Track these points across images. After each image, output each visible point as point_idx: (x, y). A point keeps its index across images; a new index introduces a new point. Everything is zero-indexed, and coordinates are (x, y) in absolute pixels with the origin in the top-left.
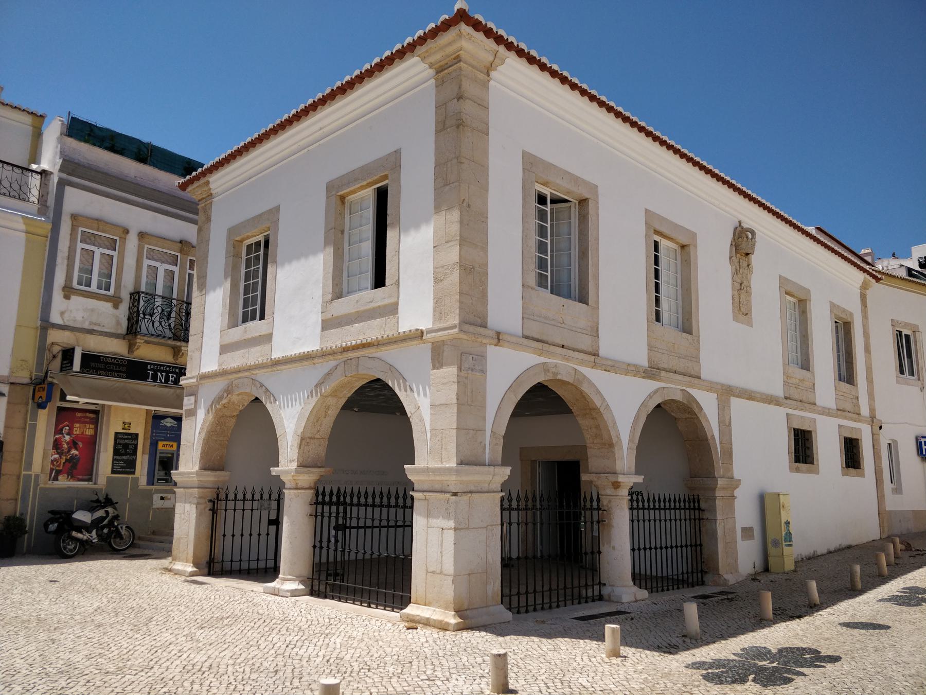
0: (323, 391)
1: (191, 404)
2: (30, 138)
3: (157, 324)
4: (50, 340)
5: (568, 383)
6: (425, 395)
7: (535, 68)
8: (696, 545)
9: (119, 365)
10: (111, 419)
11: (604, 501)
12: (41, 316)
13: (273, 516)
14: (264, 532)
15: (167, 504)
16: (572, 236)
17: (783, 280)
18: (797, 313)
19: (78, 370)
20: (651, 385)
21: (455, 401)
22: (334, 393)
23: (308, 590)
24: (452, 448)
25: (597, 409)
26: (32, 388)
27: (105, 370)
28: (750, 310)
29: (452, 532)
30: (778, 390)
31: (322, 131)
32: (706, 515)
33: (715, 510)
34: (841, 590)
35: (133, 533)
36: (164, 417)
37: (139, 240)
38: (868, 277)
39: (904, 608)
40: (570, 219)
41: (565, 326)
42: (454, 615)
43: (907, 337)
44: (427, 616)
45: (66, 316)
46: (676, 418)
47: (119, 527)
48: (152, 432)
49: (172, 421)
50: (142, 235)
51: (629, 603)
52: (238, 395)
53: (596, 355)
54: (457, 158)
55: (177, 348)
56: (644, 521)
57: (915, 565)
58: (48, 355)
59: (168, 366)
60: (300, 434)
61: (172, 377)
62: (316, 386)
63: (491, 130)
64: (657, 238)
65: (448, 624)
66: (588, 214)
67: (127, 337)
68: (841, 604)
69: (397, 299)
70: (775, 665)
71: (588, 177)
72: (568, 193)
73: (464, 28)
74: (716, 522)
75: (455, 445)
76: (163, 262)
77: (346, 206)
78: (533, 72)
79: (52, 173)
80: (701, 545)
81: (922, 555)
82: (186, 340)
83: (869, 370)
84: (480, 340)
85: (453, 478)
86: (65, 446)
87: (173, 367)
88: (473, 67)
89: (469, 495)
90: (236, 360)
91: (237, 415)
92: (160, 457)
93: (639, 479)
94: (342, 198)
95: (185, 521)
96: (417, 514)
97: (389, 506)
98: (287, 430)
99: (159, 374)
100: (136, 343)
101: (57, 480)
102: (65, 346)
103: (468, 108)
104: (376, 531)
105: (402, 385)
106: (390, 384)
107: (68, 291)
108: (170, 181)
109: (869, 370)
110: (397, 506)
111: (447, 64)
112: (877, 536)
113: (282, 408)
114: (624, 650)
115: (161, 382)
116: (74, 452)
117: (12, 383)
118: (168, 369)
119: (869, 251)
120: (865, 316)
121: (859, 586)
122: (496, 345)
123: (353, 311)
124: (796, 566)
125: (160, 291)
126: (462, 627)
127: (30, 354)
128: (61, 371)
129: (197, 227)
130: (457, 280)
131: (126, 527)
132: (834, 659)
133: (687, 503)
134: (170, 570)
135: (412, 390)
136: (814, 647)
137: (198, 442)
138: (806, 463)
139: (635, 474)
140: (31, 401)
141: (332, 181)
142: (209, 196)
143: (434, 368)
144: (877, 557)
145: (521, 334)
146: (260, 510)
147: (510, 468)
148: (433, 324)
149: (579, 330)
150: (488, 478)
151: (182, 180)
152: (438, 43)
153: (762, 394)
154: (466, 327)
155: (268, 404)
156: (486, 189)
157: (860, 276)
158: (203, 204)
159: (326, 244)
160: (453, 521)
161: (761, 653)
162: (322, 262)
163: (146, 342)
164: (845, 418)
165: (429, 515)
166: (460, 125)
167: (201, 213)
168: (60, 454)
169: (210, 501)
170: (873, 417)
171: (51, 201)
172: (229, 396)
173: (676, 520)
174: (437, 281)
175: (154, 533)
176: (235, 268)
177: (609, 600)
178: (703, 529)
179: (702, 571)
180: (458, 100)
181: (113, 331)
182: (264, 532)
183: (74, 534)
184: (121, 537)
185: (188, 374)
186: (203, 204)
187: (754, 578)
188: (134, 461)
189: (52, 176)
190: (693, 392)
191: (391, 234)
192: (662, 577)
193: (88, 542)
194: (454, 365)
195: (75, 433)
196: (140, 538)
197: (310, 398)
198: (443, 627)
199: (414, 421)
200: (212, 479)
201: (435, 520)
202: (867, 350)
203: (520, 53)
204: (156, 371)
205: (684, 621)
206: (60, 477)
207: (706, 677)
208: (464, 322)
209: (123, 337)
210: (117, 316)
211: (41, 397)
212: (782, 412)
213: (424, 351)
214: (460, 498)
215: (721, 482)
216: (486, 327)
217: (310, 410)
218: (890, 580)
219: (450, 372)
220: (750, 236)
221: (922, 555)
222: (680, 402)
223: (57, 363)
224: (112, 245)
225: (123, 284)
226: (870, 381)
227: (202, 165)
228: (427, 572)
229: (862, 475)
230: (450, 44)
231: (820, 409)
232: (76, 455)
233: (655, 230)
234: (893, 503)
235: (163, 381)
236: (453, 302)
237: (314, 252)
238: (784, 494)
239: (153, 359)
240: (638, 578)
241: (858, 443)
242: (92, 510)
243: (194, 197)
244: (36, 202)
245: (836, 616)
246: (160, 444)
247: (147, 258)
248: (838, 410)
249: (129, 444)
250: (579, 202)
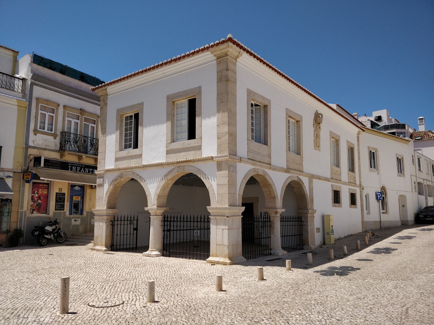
0: (168, 178)
1: (101, 182)
3: (73, 146)
4: (29, 153)
5: (261, 175)
6: (214, 181)
7: (252, 57)
8: (301, 235)
9: (57, 164)
10: (54, 187)
11: (272, 219)
13: (135, 227)
14: (132, 233)
16: (261, 119)
17: (331, 132)
18: (335, 145)
20: (288, 175)
22: (172, 179)
23: (162, 254)
24: (227, 200)
25: (270, 185)
26: (22, 174)
27: (52, 166)
29: (227, 230)
30: (329, 176)
31: (164, 74)
32: (304, 223)
34: (353, 250)
37: (64, 109)
38: (360, 130)
39: (376, 255)
41: (260, 154)
42: (228, 260)
43: (373, 153)
44: (218, 260)
45: (35, 143)
47: (61, 233)
48: (71, 193)
49: (79, 187)
50: (65, 107)
51: (281, 256)
52: (124, 178)
53: (270, 165)
54: (227, 92)
57: (377, 241)
61: (79, 168)
62: (165, 176)
63: (237, 82)
64: (289, 118)
65: (227, 263)
67: (60, 151)
68: (355, 254)
70: (341, 271)
71: (267, 97)
72: (261, 103)
73: (230, 44)
74: (308, 226)
75: (228, 199)
76: (73, 119)
77: (175, 105)
78: (251, 58)
81: (379, 237)
82: (96, 154)
83: (359, 166)
86: (36, 199)
87: (79, 164)
89: (233, 217)
90: (123, 164)
91: (122, 186)
92: (74, 203)
93: (284, 210)
94: (174, 102)
98: (151, 193)
99: (73, 167)
100: (65, 154)
101: (33, 213)
102: (35, 155)
103: (230, 73)
104: (182, 232)
105: (204, 177)
107: (36, 132)
108: (89, 87)
109: (359, 166)
110: (177, 221)
111: (222, 56)
112: (361, 231)
113: (149, 184)
114: (292, 269)
115: (74, 171)
116: (39, 201)
117: (14, 172)
118: (77, 165)
119: (356, 114)
121: (359, 248)
122: (239, 162)
123: (181, 147)
124: (335, 243)
125: (72, 131)
126: (231, 263)
127: (21, 159)
129: (100, 107)
130: (227, 138)
134: (94, 249)
135: (208, 179)
137: (105, 197)
138: (337, 203)
139: (282, 208)
140: (22, 180)
141: (169, 95)
143: (218, 171)
146: (130, 224)
147: (245, 207)
148: (217, 154)
150: (238, 211)
151: (93, 87)
152: (219, 48)
153: (324, 177)
154: (231, 156)
155: (141, 182)
157: (357, 130)
158: (103, 98)
159: (168, 120)
160: (227, 226)
161: (335, 268)
162: (166, 127)
163: (69, 154)
164: (351, 185)
165: (217, 224)
166: (227, 80)
167: (102, 101)
168: (34, 202)
169: (111, 221)
170: (360, 185)
171: (27, 92)
172: (121, 179)
174: (218, 138)
175: (72, 235)
176: (121, 126)
177: (274, 255)
178: (303, 229)
179: (303, 244)
180: (227, 71)
181: (54, 149)
182: (132, 233)
183: (45, 236)
184: (62, 237)
185: (98, 169)
186: (103, 98)
187: (321, 247)
188: (64, 205)
189: (27, 81)
190: (301, 177)
191: (197, 119)
192: (286, 247)
193: (50, 239)
195: (40, 193)
196: (69, 238)
198: (225, 264)
199: (210, 191)
200: (111, 212)
201: (220, 226)
202: (359, 159)
203: (248, 52)
204: (72, 166)
207: (321, 274)
208: (230, 154)
209: (58, 151)
211: (28, 178)
212: (329, 184)
213: (214, 164)
215: (310, 211)
217: (162, 185)
219: (225, 173)
220: (320, 116)
221: (379, 237)
222: (296, 181)
224: (94, 122)
226: (360, 171)
227: (105, 83)
228: (217, 245)
229: (356, 208)
230: (224, 49)
231: (343, 182)
232: (40, 203)
233: (289, 116)
234: (367, 218)
236: (226, 146)
237: (162, 123)
238: (332, 215)
241: (355, 195)
242: (51, 226)
246: (74, 197)
247: (67, 117)
248: (349, 182)
249: (62, 198)
250: (264, 106)
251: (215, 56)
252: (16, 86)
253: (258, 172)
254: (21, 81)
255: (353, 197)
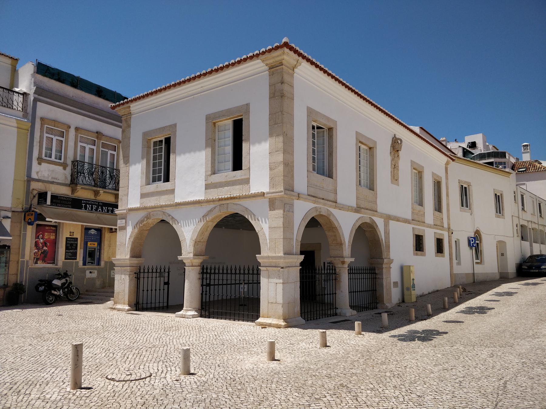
0: (208, 219)
2: (10, 71)
3: (87, 178)
4: (32, 188)
5: (325, 216)
6: (266, 222)
8: (374, 290)
9: (68, 201)
11: (337, 270)
12: (27, 174)
13: (166, 281)
14: (162, 288)
15: (113, 277)
16: (325, 145)
19: (50, 204)
21: (282, 226)
22: (212, 221)
23: (199, 315)
24: (281, 248)
27: (60, 203)
28: (398, 178)
29: (281, 285)
30: (409, 217)
33: (383, 274)
35: (79, 292)
36: (90, 229)
38: (449, 159)
39: (468, 315)
40: (324, 137)
43: (465, 188)
44: (270, 322)
45: (40, 174)
46: (365, 231)
47: (72, 288)
48: (85, 237)
50: (77, 129)
52: (152, 220)
53: (336, 202)
54: (282, 112)
55: (97, 191)
56: (353, 279)
58: (31, 196)
59: (92, 201)
60: (194, 240)
61: (95, 207)
62: (203, 217)
63: (295, 98)
64: (360, 144)
65: (281, 325)
66: (333, 135)
67: (71, 185)
68: (441, 314)
69: (249, 177)
70: (423, 335)
71: (333, 117)
72: (324, 125)
73: (286, 50)
74: (383, 279)
76: (88, 144)
78: (312, 68)
79: (29, 94)
80: (376, 290)
81: (471, 294)
83: (448, 205)
84: (292, 197)
85: (282, 260)
86: (41, 245)
88: (288, 67)
90: (151, 202)
93: (353, 260)
94: (214, 124)
95: (122, 283)
96: (262, 277)
97: (231, 274)
99: (88, 205)
101: (37, 263)
102: (39, 190)
103: (286, 87)
104: (225, 286)
106: (246, 217)
107: (40, 160)
108: (106, 104)
109: (448, 205)
110: (219, 273)
111: (275, 65)
113: (183, 227)
114: (363, 333)
115: (89, 210)
116: (45, 248)
117: (13, 211)
118: (92, 203)
120: (447, 178)
121: (447, 307)
127: (22, 195)
128: (38, 204)
129: (121, 129)
131: (76, 288)
132: (446, 333)
133: (351, 271)
134: (114, 309)
135: (258, 220)
136: (436, 329)
137: (129, 243)
140: (23, 221)
141: (209, 114)
142: (129, 113)
144: (454, 294)
145: (306, 193)
147: (304, 256)
149: (329, 191)
150: (296, 260)
151: (113, 104)
152: (272, 55)
154: (287, 192)
156: (292, 126)
157: (445, 159)
159: (207, 146)
161: (416, 332)
163: (82, 188)
164: (437, 229)
165: (269, 277)
166: (282, 96)
167: (124, 122)
169: (135, 273)
170: (449, 228)
171: (30, 110)
172: (148, 220)
173: (366, 279)
174: (271, 169)
175: (87, 291)
176: (148, 153)
179: (376, 302)
181: (63, 182)
182: (162, 288)
183: (53, 292)
184: (73, 293)
185: (119, 208)
187: (399, 305)
188: (76, 253)
189: (29, 96)
190: (374, 218)
194: (281, 209)
197: (200, 222)
198: (279, 327)
200: (136, 262)
202: (447, 195)
203: (308, 60)
204: (86, 204)
205: (382, 321)
206: (38, 262)
207: (399, 340)
208: (285, 189)
209: (69, 185)
210: (66, 174)
211: (30, 219)
212: (410, 226)
213: (265, 203)
214: (285, 270)
215: (385, 261)
216: (293, 191)
218: (459, 304)
220: (399, 142)
221: (471, 294)
222: (369, 223)
223: (36, 200)
225: (68, 157)
226: (448, 210)
228: (269, 303)
229: (444, 256)
230: (278, 56)
232: (46, 250)
234: (457, 270)
235: (90, 209)
237: (200, 150)
238: (413, 266)
239: (83, 197)
240: (352, 307)
241: (442, 241)
242: (60, 279)
243: (120, 113)
244: (21, 111)
245: (440, 319)
246: (89, 243)
247: (80, 142)
248: (434, 225)
251: (267, 65)
252: (15, 103)
253: (320, 212)
254: (22, 96)
255: (439, 243)
